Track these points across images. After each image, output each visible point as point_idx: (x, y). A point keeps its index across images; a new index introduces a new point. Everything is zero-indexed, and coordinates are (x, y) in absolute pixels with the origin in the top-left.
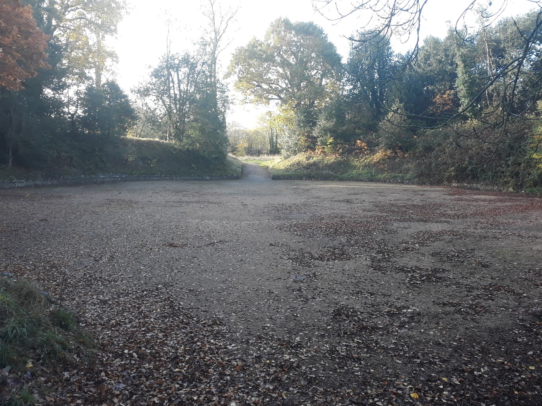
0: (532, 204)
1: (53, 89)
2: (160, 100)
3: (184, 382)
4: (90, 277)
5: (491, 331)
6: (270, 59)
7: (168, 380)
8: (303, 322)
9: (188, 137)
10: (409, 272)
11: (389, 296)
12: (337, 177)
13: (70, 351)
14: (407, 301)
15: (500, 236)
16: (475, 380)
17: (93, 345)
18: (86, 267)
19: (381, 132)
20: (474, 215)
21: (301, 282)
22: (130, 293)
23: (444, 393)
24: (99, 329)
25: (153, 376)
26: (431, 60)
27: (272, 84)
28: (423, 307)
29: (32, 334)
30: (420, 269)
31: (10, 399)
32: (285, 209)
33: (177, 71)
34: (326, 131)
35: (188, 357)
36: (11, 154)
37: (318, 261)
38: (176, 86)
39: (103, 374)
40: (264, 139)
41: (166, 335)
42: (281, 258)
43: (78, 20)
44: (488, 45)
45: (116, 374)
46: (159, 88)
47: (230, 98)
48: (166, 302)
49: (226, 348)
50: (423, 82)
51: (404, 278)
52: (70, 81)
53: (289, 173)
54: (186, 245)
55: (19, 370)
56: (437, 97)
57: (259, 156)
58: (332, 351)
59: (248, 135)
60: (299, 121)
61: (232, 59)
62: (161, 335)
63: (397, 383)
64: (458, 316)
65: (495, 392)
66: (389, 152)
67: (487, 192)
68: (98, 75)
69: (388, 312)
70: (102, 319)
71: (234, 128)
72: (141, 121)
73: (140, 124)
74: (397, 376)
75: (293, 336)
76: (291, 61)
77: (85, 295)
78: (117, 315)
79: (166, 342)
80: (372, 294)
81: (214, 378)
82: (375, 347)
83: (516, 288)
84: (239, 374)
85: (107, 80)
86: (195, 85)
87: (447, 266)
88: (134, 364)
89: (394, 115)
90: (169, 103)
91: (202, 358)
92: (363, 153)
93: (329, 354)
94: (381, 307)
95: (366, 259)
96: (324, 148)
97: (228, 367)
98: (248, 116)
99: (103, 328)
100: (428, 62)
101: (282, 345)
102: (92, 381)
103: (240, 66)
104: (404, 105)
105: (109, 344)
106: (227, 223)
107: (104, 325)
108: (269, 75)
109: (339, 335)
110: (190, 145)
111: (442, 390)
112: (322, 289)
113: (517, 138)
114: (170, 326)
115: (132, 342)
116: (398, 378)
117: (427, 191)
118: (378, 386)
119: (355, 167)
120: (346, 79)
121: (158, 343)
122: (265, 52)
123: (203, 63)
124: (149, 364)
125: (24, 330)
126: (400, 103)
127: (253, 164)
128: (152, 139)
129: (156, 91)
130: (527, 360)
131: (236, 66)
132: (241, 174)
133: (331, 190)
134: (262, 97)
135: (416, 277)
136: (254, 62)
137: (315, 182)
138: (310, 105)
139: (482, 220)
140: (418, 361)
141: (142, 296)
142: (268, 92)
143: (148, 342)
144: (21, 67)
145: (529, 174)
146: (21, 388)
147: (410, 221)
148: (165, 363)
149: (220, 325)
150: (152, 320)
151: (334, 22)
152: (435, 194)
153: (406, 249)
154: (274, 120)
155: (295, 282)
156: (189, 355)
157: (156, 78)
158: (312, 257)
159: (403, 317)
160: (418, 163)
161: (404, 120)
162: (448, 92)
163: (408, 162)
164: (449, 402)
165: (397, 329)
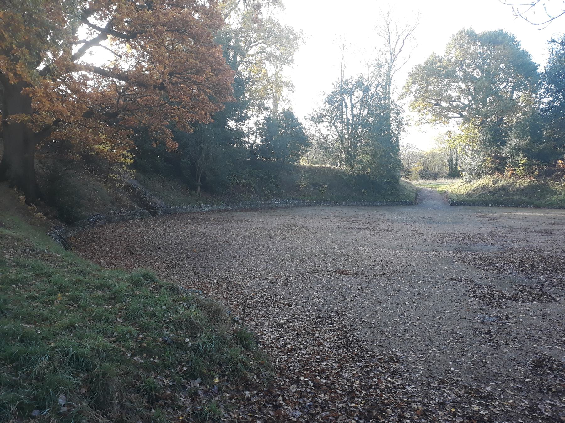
1: (236, 121)
2: (333, 126)
3: (360, 419)
4: (267, 299)
6: (450, 75)
7: (344, 414)
8: (495, 371)
9: (360, 161)
12: (532, 203)
13: (251, 371)
17: (271, 368)
18: (263, 289)
21: (490, 324)
22: (304, 319)
24: (276, 352)
25: (329, 407)
27: (453, 101)
29: (219, 350)
31: (201, 410)
32: (468, 240)
33: (350, 96)
34: (517, 150)
35: (364, 393)
36: (199, 182)
37: (511, 301)
38: (349, 110)
39: (280, 398)
40: (442, 161)
41: (341, 366)
42: (465, 295)
43: (260, 54)
45: (292, 400)
46: (332, 114)
47: (404, 120)
48: (340, 331)
49: (404, 388)
52: (250, 113)
53: (471, 199)
54: (357, 273)
55: (208, 384)
57: (435, 179)
58: (533, 409)
59: (424, 157)
60: (485, 140)
61: (408, 78)
62: (335, 366)
68: (275, 105)
70: (278, 342)
71: (408, 151)
72: (314, 148)
73: (312, 150)
75: (483, 386)
76: (475, 75)
77: (262, 317)
78: (292, 339)
79: (340, 373)
81: (393, 420)
84: (420, 419)
85: (284, 109)
86: (368, 109)
88: (310, 393)
90: (341, 129)
91: (379, 396)
93: (529, 412)
96: (515, 170)
97: (407, 409)
98: (423, 137)
99: (279, 352)
101: (470, 393)
102: (271, 404)
103: (417, 85)
105: (285, 369)
106: (400, 253)
107: (280, 349)
108: (450, 92)
110: (361, 170)
114: (345, 357)
115: (307, 370)
119: (555, 192)
120: (543, 90)
121: (333, 374)
122: (445, 68)
123: (378, 86)
124: (325, 394)
125: (213, 346)
127: (429, 189)
128: (323, 165)
129: (329, 118)
131: (413, 85)
132: (415, 199)
133: (524, 218)
134: (442, 116)
136: (432, 79)
137: (504, 209)
138: (497, 122)
141: (315, 323)
142: (448, 110)
143: (323, 371)
144: (211, 101)
146: (210, 401)
148: (341, 396)
149: (397, 362)
150: (327, 349)
151: (541, 26)
154: (455, 140)
155: (483, 323)
156: (366, 391)
157: (329, 104)
158: (503, 296)
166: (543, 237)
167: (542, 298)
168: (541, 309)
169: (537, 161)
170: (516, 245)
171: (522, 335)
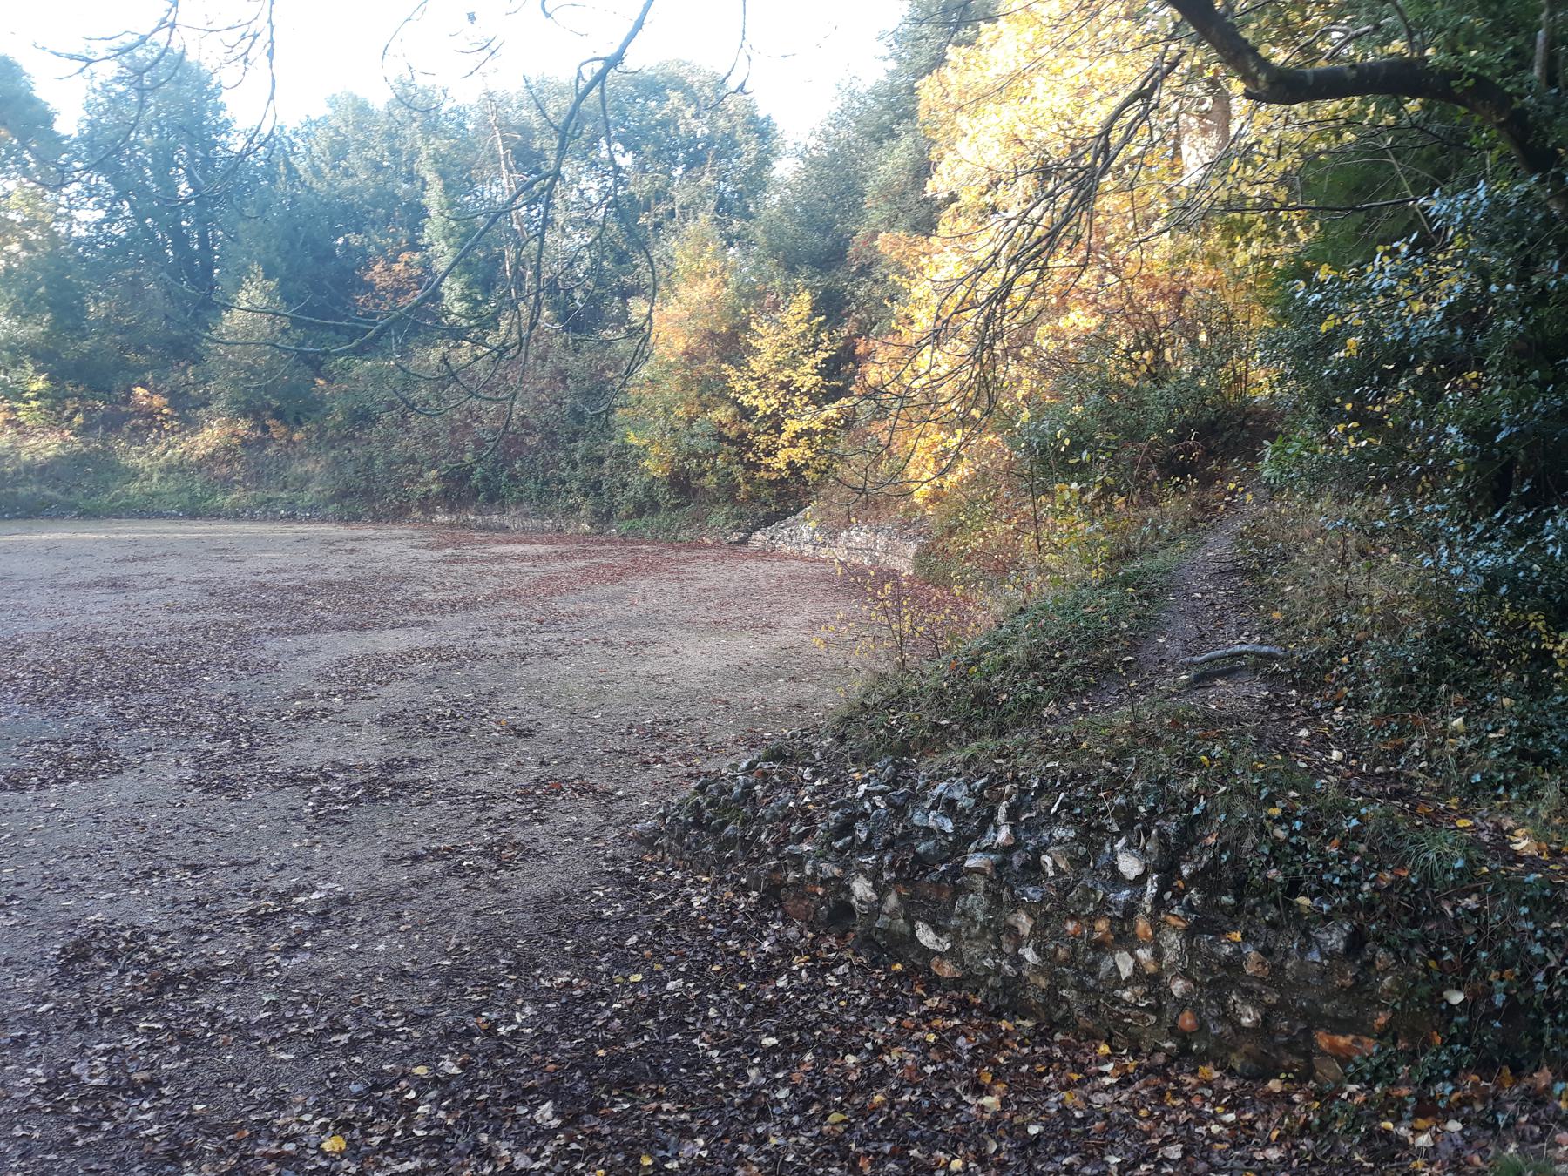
0: (635, 561)
5: (539, 906)
10: (314, 781)
11: (253, 863)
12: (74, 506)
14: (307, 869)
15: (560, 650)
16: (501, 1052)
19: (211, 361)
20: (495, 599)
23: (420, 1109)
26: (352, 158)
28: (356, 878)
30: (347, 769)
44: (503, 138)
50: (332, 223)
51: (300, 802)
56: (377, 268)
63: (279, 1122)
64: (454, 883)
65: (551, 1067)
66: (243, 426)
67: (527, 536)
69: (250, 913)
74: (280, 1102)
80: (196, 869)
82: (207, 1031)
83: (601, 781)
87: (422, 748)
89: (248, 308)
92: (160, 428)
93: (45, 1097)
94: (227, 903)
95: (178, 763)
96: (14, 410)
100: (343, 164)
104: (282, 284)
109: (82, 1025)
111: (415, 1103)
112: (18, 884)
113: (589, 393)
116: (283, 1109)
117: (365, 539)
118: (220, 1152)
119: (134, 474)
126: (267, 277)
130: (623, 962)
133: (52, 549)
135: (333, 795)
139: (515, 611)
140: (343, 1039)
145: (624, 486)
147: (317, 631)
152: (389, 547)
153: (306, 715)
159: (297, 919)
160: (335, 458)
161: (284, 331)
162: (405, 256)
163: (304, 456)
164: (433, 1133)
165: (278, 959)
166: (103, 597)
167: (93, 768)
168: (90, 796)
169: (77, 386)
170: (24, 628)
171: (32, 885)
